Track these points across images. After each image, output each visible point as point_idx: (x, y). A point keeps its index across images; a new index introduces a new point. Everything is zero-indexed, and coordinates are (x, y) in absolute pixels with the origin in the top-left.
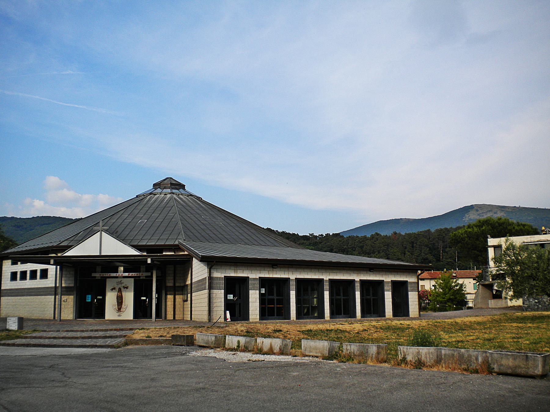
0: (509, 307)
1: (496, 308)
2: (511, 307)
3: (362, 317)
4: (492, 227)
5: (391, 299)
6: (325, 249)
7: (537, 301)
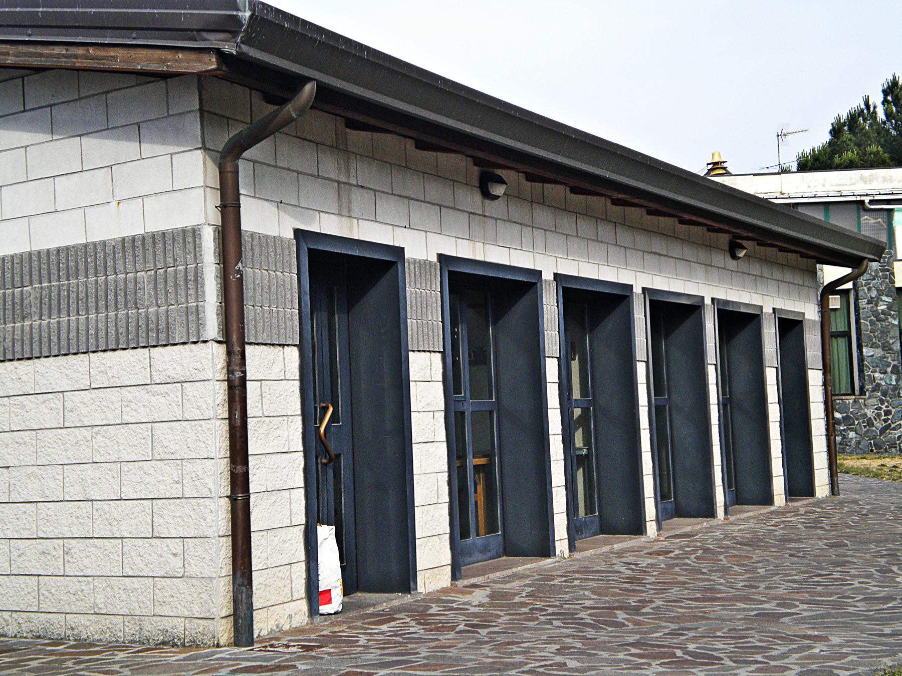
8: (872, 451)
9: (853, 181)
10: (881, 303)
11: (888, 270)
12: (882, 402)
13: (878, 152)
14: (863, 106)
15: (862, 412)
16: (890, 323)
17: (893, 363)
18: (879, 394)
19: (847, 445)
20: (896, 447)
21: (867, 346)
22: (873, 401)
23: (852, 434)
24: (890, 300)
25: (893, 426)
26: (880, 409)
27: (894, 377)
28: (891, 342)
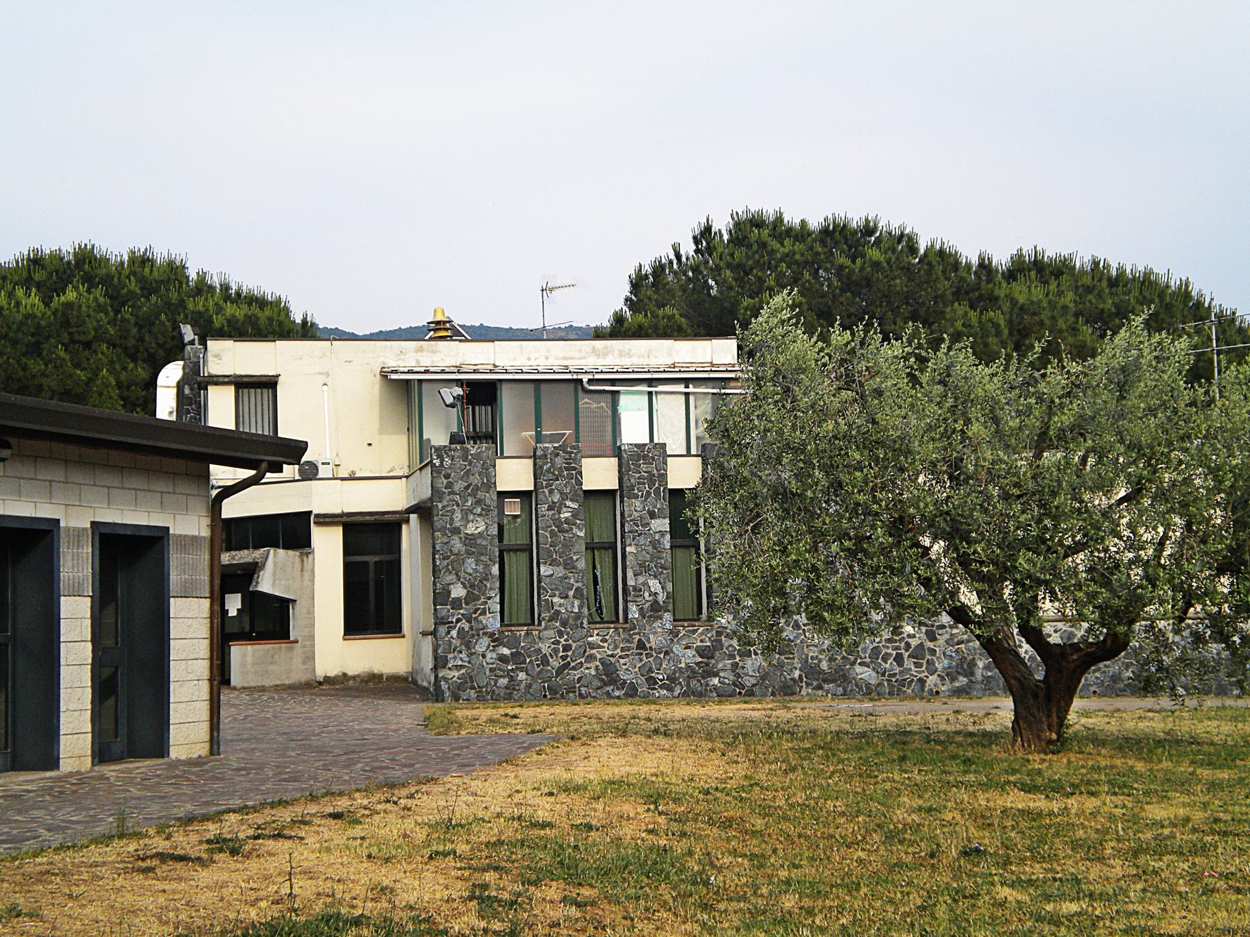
0: (320, 683)
1: (263, 689)
2: (327, 680)
3: (102, 754)
4: (111, 297)
5: (89, 646)
6: (403, 338)
7: (506, 651)
8: (545, 696)
9: (584, 354)
10: (565, 509)
11: (575, 469)
12: (561, 634)
13: (673, 315)
14: (672, 256)
15: (536, 647)
16: (575, 535)
17: (576, 585)
18: (557, 624)
19: (514, 689)
20: (575, 692)
21: (545, 563)
22: (550, 633)
23: (522, 676)
24: (575, 505)
25: (572, 664)
26: (558, 642)
27: (576, 603)
28: (575, 558)
